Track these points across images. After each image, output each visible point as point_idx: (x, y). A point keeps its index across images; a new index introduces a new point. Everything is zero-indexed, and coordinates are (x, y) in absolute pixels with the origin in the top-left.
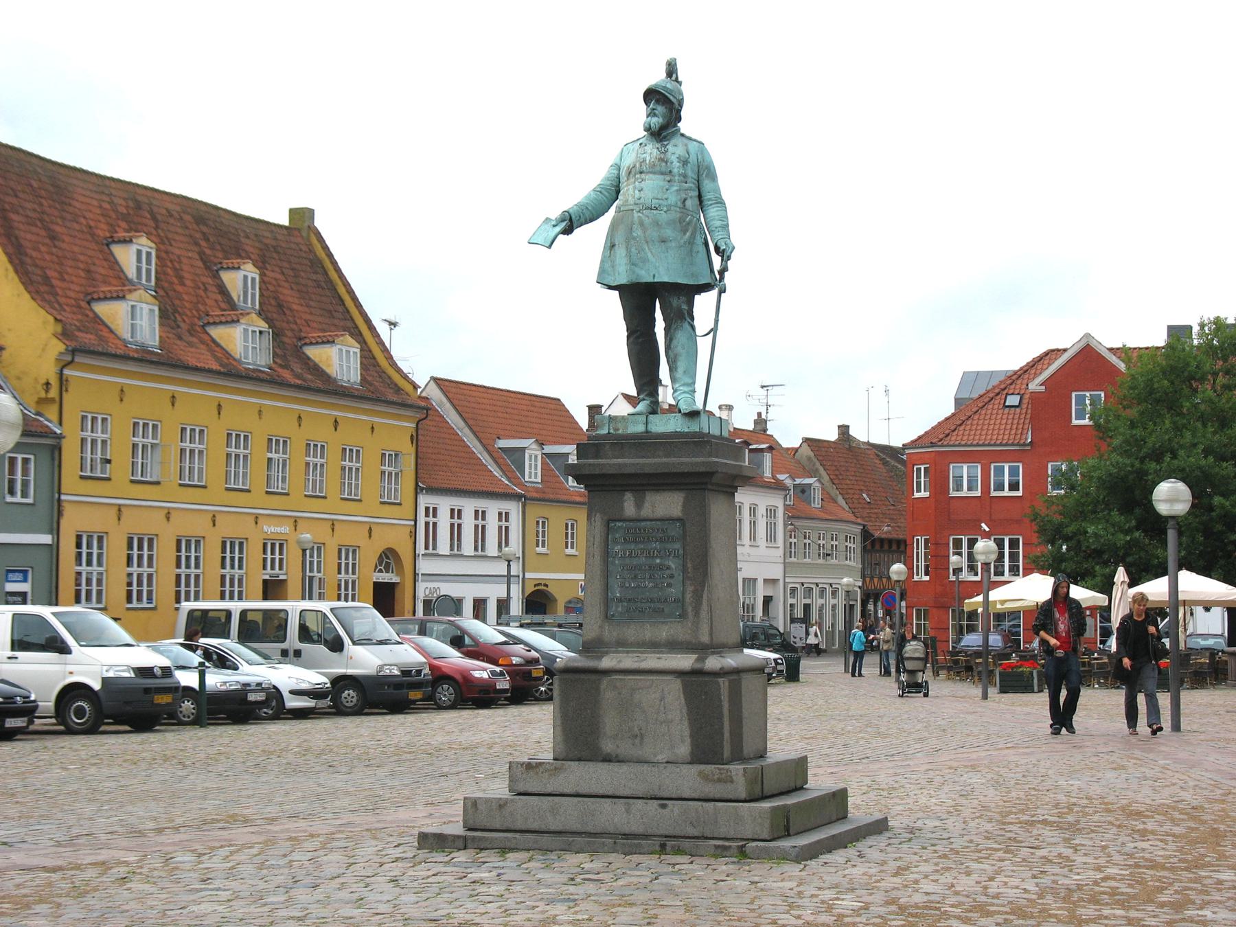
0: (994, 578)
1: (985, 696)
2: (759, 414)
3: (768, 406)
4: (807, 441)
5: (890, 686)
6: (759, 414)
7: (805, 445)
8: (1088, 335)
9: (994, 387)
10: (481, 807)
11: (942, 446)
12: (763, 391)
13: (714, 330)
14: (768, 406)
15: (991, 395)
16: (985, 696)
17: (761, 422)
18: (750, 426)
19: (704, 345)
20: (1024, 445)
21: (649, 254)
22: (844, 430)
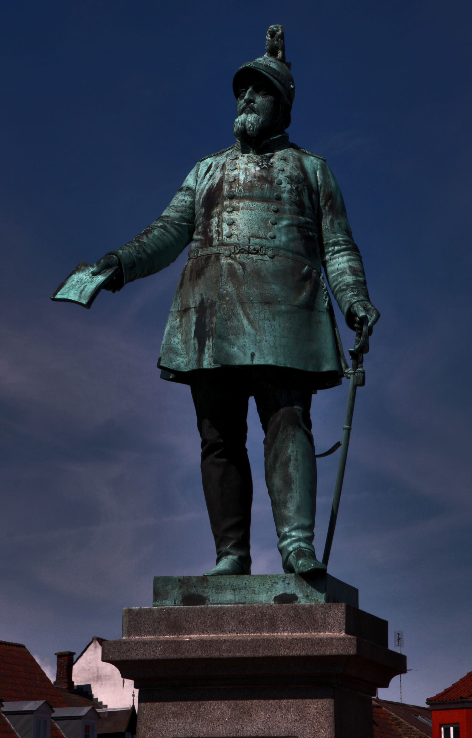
21: (245, 322)
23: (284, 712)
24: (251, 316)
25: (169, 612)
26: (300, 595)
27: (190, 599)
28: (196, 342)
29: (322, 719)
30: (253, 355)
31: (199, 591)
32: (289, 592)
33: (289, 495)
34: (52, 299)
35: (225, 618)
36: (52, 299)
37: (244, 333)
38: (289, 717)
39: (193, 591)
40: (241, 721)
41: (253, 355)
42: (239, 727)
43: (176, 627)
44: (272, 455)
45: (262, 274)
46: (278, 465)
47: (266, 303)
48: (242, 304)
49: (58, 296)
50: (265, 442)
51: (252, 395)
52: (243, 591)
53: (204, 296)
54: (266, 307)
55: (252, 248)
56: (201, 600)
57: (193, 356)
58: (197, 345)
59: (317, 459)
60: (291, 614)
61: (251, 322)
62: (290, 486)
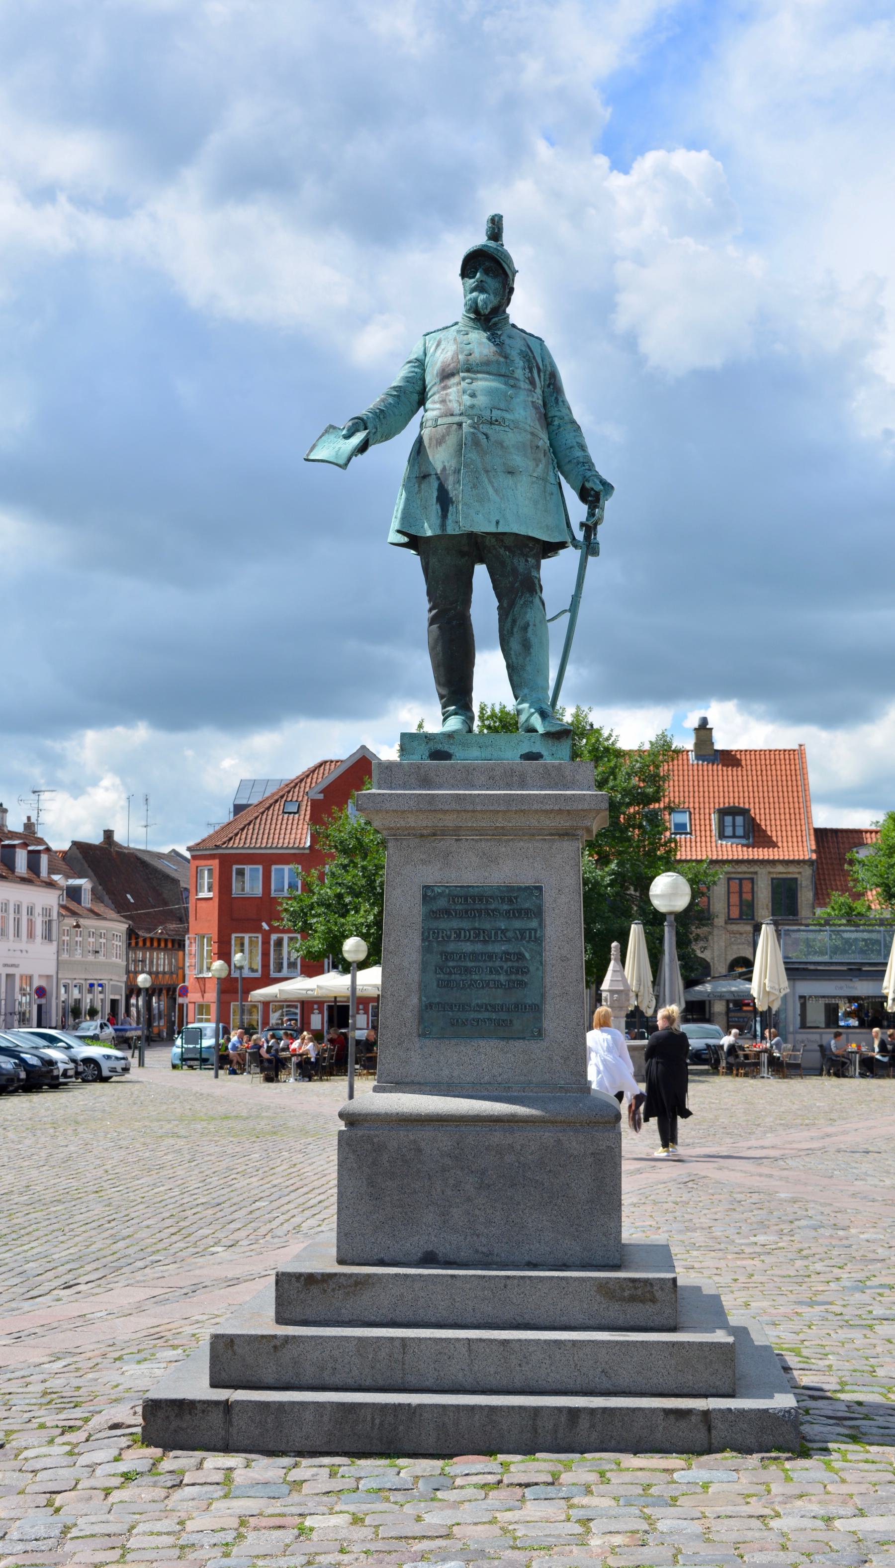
0: (273, 975)
1: (217, 1076)
2: (29, 818)
3: (39, 810)
4: (75, 844)
5: (260, 1077)
6: (29, 818)
7: (75, 847)
8: (363, 747)
9: (273, 795)
10: (717, 1423)
11: (226, 848)
12: (35, 797)
13: (574, 608)
14: (39, 810)
15: (276, 798)
16: (217, 1076)
17: (29, 826)
18: (20, 829)
19: (556, 632)
20: (304, 848)
21: (491, 490)
22: (108, 834)
23: (531, 861)
24: (495, 485)
25: (419, 767)
26: (545, 753)
27: (439, 755)
28: (438, 507)
29: (568, 868)
30: (497, 523)
31: (446, 748)
32: (534, 751)
33: (528, 659)
34: (305, 460)
35: (475, 773)
36: (305, 460)
37: (489, 500)
38: (536, 865)
39: (439, 747)
40: (488, 869)
41: (497, 523)
42: (487, 874)
43: (426, 782)
44: (509, 620)
45: (505, 444)
46: (515, 630)
47: (509, 473)
48: (487, 472)
49: (311, 457)
50: (500, 608)
51: (481, 561)
52: (490, 748)
53: (446, 464)
54: (509, 476)
55: (494, 419)
56: (447, 756)
57: (436, 520)
58: (439, 511)
59: (549, 624)
60: (541, 771)
61: (496, 491)
62: (529, 650)
